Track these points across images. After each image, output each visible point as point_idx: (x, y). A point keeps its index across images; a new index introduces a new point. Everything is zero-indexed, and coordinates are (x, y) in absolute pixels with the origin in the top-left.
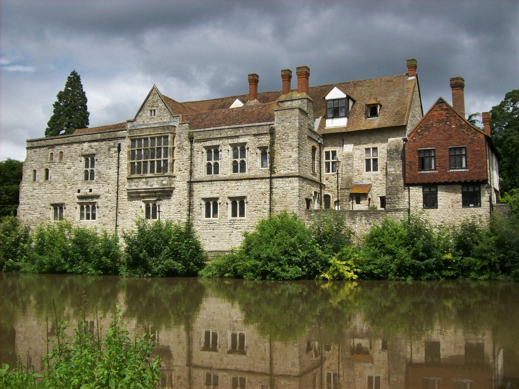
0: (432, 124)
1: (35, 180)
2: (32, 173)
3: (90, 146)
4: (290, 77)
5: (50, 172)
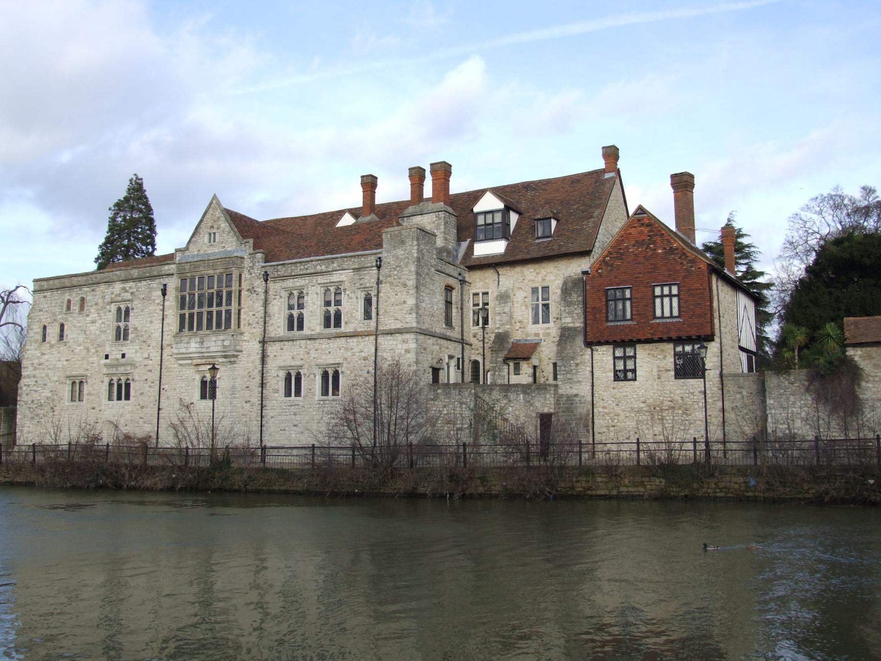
0: (627, 248)
1: (44, 340)
2: (40, 330)
3: (124, 289)
4: (422, 177)
5: (66, 327)
